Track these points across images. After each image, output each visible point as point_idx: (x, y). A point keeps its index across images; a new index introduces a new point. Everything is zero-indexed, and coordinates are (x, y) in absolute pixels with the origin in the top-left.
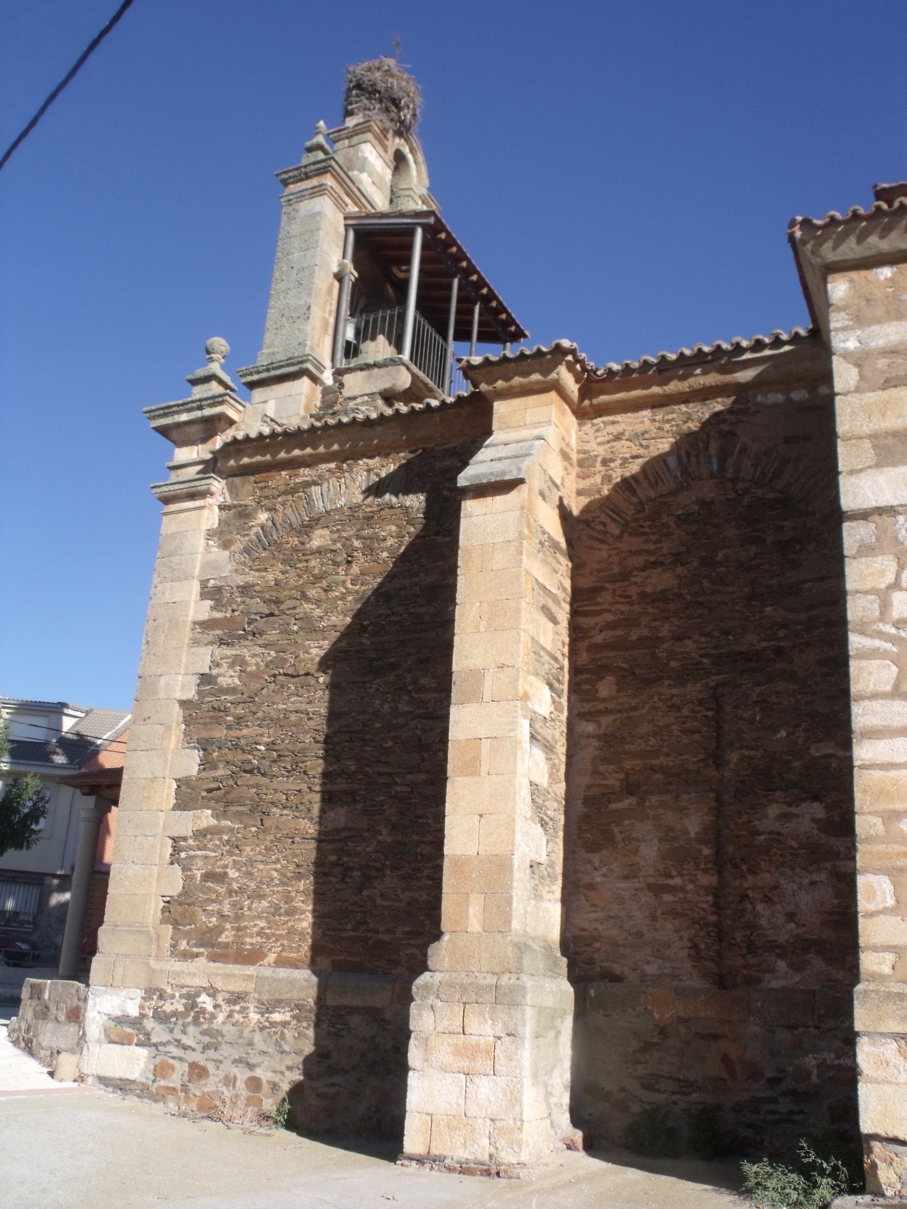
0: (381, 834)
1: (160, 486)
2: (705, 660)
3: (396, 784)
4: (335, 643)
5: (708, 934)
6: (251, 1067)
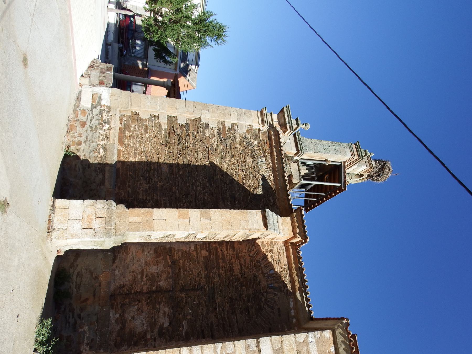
0: (160, 183)
1: (266, 110)
2: (212, 284)
3: (175, 187)
5: (128, 290)
6: (85, 142)
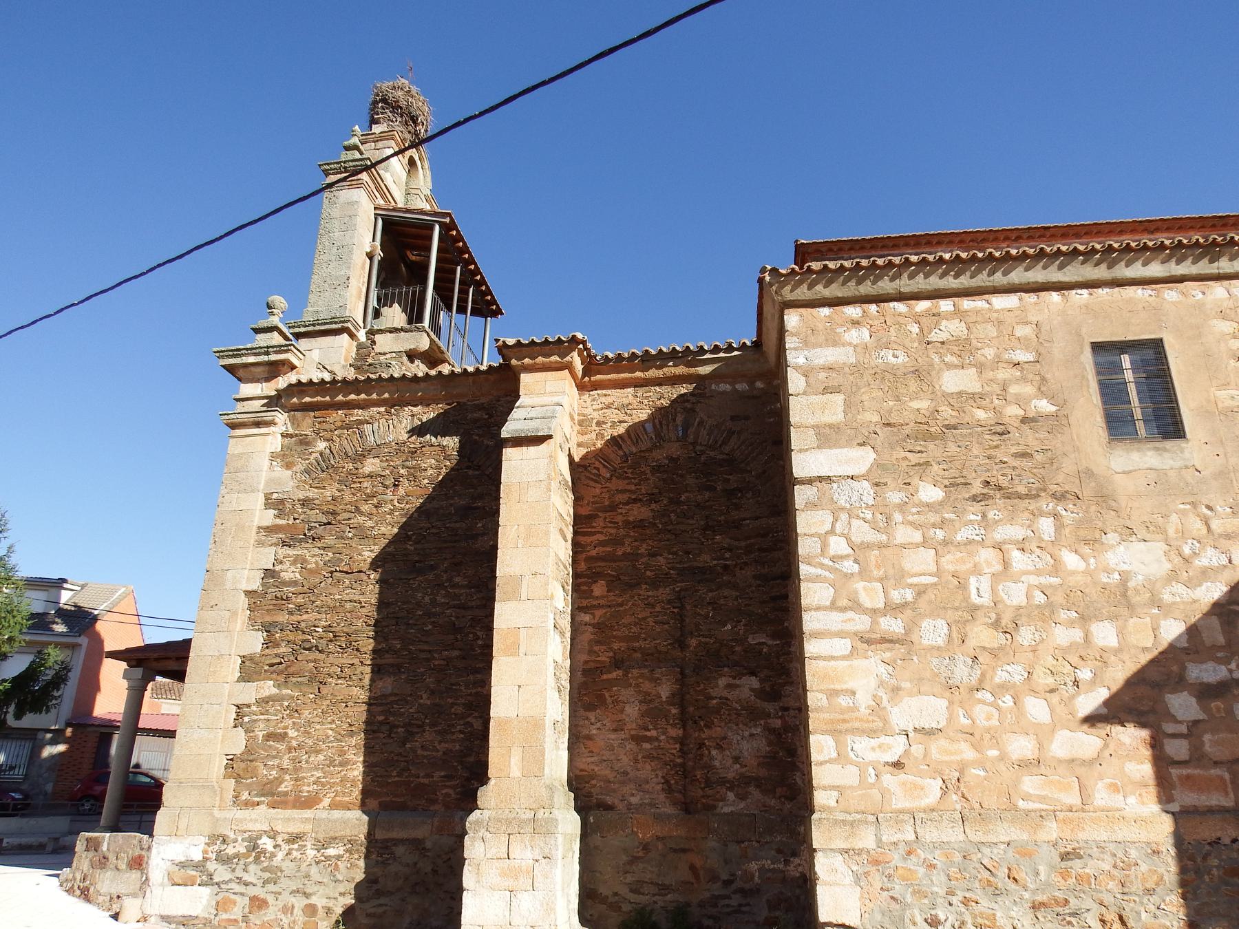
1: (228, 414)
2: (672, 572)
3: (434, 658)
4: (384, 548)
5: (677, 772)
6: (307, 895)
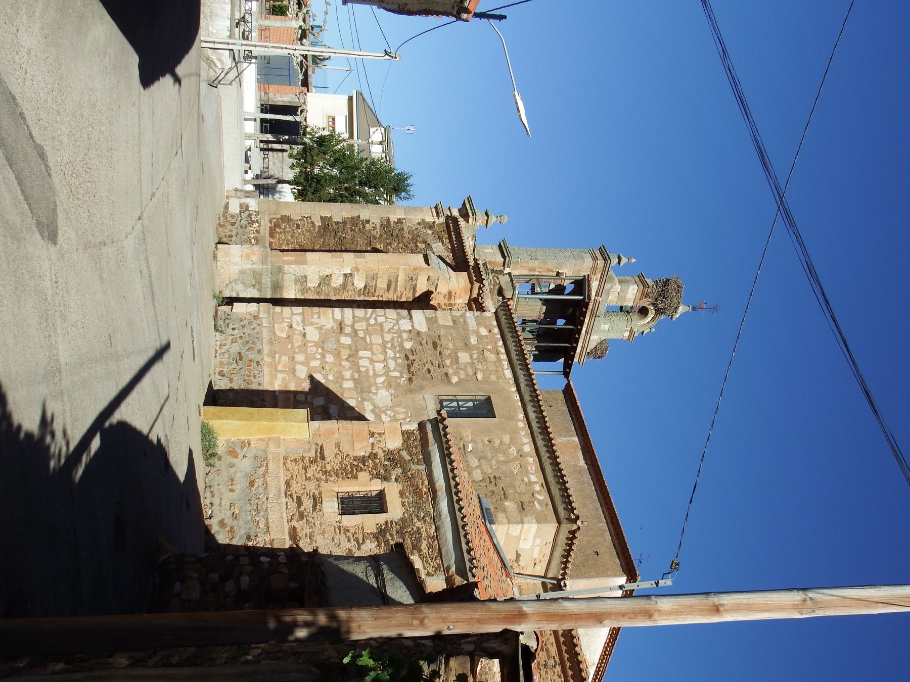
6: (236, 236)
